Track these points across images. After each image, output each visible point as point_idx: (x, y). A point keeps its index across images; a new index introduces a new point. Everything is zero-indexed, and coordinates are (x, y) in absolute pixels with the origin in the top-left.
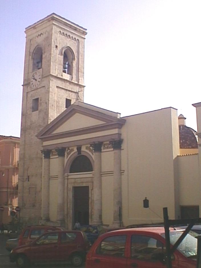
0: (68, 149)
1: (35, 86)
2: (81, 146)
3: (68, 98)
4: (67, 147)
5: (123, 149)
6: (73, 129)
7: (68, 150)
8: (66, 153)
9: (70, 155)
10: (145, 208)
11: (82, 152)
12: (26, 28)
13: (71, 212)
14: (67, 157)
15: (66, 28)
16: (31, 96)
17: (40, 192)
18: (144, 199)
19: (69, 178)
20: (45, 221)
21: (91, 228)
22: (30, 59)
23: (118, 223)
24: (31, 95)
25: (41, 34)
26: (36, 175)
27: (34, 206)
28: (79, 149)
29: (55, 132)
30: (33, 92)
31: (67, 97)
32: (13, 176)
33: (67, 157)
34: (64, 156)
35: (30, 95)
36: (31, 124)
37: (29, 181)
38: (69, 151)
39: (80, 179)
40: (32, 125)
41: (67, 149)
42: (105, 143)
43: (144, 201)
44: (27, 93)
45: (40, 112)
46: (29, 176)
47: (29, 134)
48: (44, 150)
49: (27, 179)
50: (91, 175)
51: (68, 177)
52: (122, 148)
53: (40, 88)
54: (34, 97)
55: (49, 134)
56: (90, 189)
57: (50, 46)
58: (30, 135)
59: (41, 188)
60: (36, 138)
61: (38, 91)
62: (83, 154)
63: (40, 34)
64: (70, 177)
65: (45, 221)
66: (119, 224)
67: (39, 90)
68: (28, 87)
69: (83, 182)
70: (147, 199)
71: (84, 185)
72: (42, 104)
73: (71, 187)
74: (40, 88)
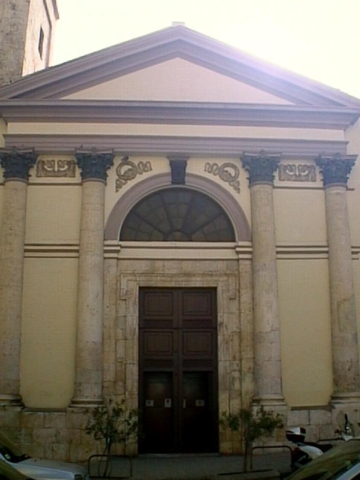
0: (126, 161)
2: (188, 156)
4: (121, 154)
6: (146, 99)
7: (121, 165)
8: (112, 175)
11: (187, 179)
12: (174, 22)
14: (118, 187)
22: (262, 148)
23: (99, 473)
28: (178, 168)
33: (118, 187)
38: (126, 168)
39: (176, 262)
41: (117, 161)
42: (285, 163)
43: (108, 176)
52: (350, 184)
62: (190, 183)
69: (188, 275)
71: (197, 282)
73: (131, 287)
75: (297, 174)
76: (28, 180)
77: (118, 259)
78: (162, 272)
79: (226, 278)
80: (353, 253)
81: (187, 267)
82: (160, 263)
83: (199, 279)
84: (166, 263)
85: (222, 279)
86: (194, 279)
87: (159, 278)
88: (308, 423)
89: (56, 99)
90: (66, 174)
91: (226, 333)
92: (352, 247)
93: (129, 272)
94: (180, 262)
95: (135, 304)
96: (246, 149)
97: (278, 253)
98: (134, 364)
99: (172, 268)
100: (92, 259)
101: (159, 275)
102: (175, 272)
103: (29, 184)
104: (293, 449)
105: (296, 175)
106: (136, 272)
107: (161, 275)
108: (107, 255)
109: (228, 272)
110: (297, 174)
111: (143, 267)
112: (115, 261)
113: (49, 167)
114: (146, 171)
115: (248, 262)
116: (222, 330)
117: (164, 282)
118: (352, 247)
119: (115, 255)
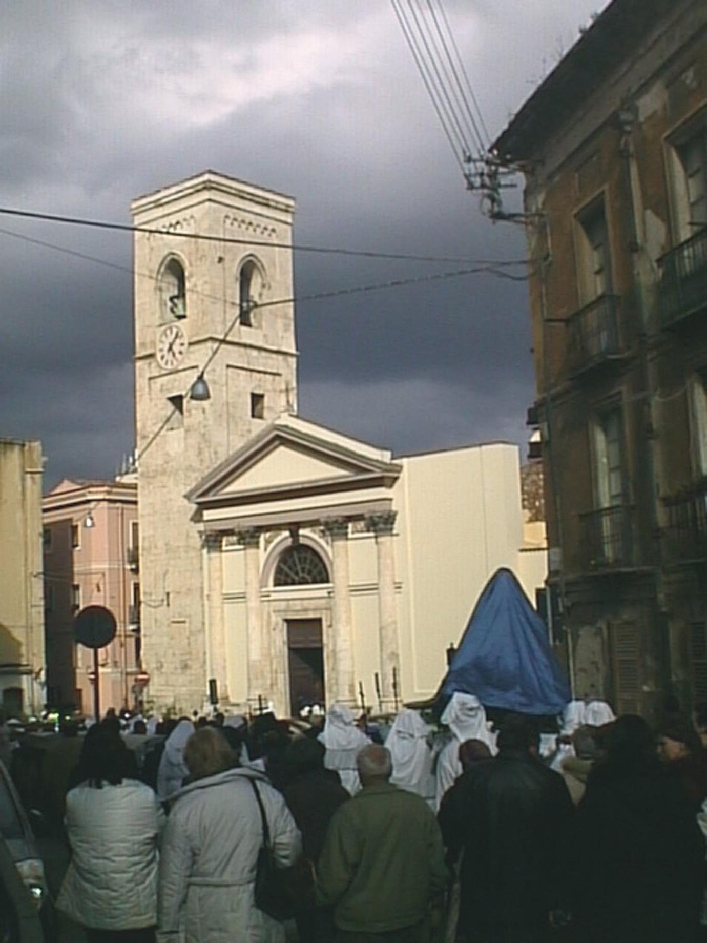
1: (169, 363)
3: (257, 392)
5: (397, 535)
9: (272, 546)
14: (266, 549)
16: (161, 390)
17: (199, 631)
18: (449, 647)
24: (162, 386)
25: (178, 223)
26: (189, 590)
27: (185, 667)
29: (229, 489)
30: (166, 378)
31: (255, 388)
32: (456, 646)
34: (257, 545)
35: (158, 386)
36: (167, 462)
40: (170, 464)
44: (150, 379)
45: (187, 431)
46: (168, 594)
47: (164, 487)
48: (205, 531)
49: (163, 600)
50: (324, 593)
53: (184, 370)
54: (172, 392)
55: (214, 495)
56: (325, 624)
57: (204, 259)
58: (165, 490)
59: (203, 624)
60: (186, 502)
62: (302, 541)
69: (306, 610)
71: (311, 615)
72: (194, 412)
74: (184, 370)
99: (298, 605)
100: (253, 602)
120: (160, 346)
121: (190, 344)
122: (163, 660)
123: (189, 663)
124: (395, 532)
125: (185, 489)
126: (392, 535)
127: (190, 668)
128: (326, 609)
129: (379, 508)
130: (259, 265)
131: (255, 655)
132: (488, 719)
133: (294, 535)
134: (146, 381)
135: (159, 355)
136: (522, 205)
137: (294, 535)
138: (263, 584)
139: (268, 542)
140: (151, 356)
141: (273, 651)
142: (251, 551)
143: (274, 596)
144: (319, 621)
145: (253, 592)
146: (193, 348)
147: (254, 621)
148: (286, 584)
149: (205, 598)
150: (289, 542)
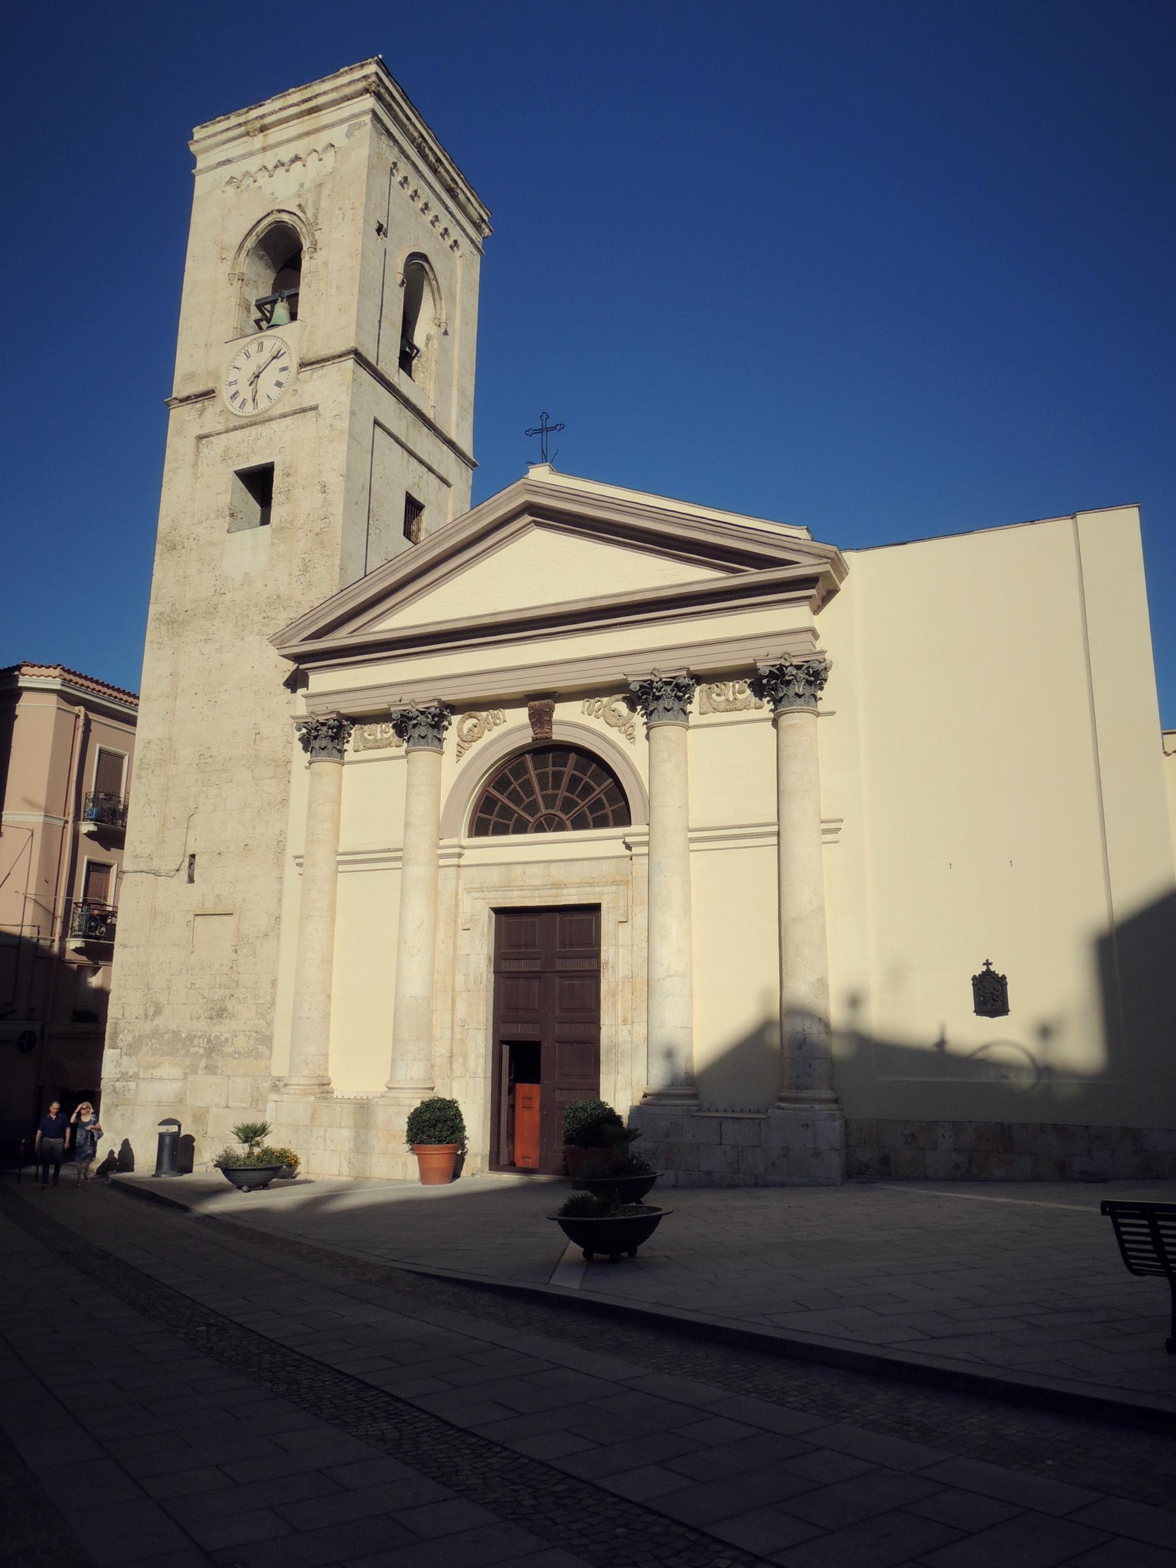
9: (476, 747)
10: (985, 1020)
13: (234, 120)
14: (459, 754)
15: (474, 797)
18: (980, 970)
19: (463, 861)
20: (312, 1098)
21: (120, 822)
25: (297, 158)
29: (373, 630)
33: (459, 754)
37: (191, 880)
39: (542, 865)
40: (228, 597)
44: (200, 438)
51: (460, 856)
61: (265, 430)
62: (559, 734)
63: (286, 159)
64: (469, 857)
65: (312, 1098)
66: (149, 987)
67: (274, 425)
68: (203, 410)
69: (557, 886)
70: (998, 969)
75: (731, 698)
76: (687, 720)
77: (459, 866)
78: (521, 884)
79: (614, 888)
80: (825, 832)
81: (557, 873)
82: (519, 869)
83: (574, 891)
84: (527, 868)
85: (607, 889)
86: (565, 891)
87: (515, 893)
88: (719, 1142)
89: (329, 638)
90: (391, 743)
91: (612, 979)
92: (823, 822)
93: (475, 886)
94: (547, 864)
95: (482, 935)
96: (627, 670)
97: (692, 840)
98: (480, 1029)
99: (536, 875)
100: (419, 870)
101: (515, 888)
102: (538, 882)
103: (688, 728)
104: (183, 1133)
105: (728, 700)
106: (485, 885)
107: (518, 888)
108: (442, 862)
109: (618, 878)
110: (731, 698)
111: (494, 876)
112: (453, 870)
113: (369, 735)
114: (496, 724)
115: (646, 859)
116: (606, 973)
117: (523, 899)
118: (823, 822)
119: (454, 861)
120: (234, 375)
121: (303, 365)
122: (163, 1000)
123: (230, 1005)
124: (821, 706)
125: (427, 531)
126: (818, 714)
127: (232, 1016)
128: (615, 883)
129: (797, 650)
130: (430, 274)
131: (415, 985)
132: (102, 995)
133: (540, 718)
134: (193, 440)
135: (225, 393)
136: (411, 543)
137: (540, 718)
138: (442, 830)
139: (465, 741)
140: (208, 394)
141: (460, 978)
142: (423, 757)
143: (469, 857)
144: (595, 908)
145: (421, 845)
146: (306, 373)
147: (418, 908)
148: (500, 830)
149: (290, 863)
150: (526, 737)
